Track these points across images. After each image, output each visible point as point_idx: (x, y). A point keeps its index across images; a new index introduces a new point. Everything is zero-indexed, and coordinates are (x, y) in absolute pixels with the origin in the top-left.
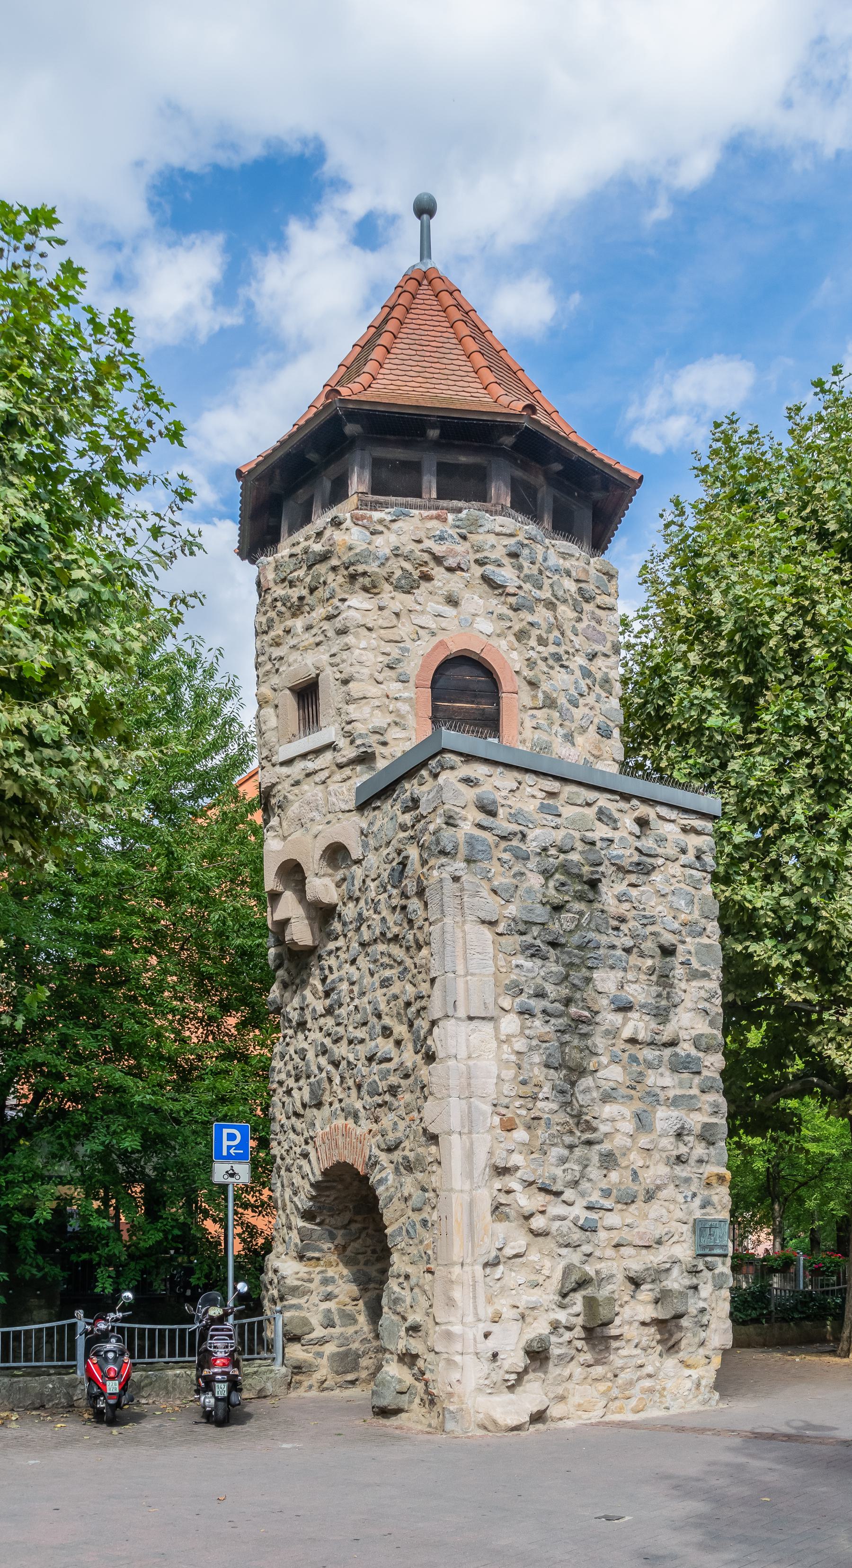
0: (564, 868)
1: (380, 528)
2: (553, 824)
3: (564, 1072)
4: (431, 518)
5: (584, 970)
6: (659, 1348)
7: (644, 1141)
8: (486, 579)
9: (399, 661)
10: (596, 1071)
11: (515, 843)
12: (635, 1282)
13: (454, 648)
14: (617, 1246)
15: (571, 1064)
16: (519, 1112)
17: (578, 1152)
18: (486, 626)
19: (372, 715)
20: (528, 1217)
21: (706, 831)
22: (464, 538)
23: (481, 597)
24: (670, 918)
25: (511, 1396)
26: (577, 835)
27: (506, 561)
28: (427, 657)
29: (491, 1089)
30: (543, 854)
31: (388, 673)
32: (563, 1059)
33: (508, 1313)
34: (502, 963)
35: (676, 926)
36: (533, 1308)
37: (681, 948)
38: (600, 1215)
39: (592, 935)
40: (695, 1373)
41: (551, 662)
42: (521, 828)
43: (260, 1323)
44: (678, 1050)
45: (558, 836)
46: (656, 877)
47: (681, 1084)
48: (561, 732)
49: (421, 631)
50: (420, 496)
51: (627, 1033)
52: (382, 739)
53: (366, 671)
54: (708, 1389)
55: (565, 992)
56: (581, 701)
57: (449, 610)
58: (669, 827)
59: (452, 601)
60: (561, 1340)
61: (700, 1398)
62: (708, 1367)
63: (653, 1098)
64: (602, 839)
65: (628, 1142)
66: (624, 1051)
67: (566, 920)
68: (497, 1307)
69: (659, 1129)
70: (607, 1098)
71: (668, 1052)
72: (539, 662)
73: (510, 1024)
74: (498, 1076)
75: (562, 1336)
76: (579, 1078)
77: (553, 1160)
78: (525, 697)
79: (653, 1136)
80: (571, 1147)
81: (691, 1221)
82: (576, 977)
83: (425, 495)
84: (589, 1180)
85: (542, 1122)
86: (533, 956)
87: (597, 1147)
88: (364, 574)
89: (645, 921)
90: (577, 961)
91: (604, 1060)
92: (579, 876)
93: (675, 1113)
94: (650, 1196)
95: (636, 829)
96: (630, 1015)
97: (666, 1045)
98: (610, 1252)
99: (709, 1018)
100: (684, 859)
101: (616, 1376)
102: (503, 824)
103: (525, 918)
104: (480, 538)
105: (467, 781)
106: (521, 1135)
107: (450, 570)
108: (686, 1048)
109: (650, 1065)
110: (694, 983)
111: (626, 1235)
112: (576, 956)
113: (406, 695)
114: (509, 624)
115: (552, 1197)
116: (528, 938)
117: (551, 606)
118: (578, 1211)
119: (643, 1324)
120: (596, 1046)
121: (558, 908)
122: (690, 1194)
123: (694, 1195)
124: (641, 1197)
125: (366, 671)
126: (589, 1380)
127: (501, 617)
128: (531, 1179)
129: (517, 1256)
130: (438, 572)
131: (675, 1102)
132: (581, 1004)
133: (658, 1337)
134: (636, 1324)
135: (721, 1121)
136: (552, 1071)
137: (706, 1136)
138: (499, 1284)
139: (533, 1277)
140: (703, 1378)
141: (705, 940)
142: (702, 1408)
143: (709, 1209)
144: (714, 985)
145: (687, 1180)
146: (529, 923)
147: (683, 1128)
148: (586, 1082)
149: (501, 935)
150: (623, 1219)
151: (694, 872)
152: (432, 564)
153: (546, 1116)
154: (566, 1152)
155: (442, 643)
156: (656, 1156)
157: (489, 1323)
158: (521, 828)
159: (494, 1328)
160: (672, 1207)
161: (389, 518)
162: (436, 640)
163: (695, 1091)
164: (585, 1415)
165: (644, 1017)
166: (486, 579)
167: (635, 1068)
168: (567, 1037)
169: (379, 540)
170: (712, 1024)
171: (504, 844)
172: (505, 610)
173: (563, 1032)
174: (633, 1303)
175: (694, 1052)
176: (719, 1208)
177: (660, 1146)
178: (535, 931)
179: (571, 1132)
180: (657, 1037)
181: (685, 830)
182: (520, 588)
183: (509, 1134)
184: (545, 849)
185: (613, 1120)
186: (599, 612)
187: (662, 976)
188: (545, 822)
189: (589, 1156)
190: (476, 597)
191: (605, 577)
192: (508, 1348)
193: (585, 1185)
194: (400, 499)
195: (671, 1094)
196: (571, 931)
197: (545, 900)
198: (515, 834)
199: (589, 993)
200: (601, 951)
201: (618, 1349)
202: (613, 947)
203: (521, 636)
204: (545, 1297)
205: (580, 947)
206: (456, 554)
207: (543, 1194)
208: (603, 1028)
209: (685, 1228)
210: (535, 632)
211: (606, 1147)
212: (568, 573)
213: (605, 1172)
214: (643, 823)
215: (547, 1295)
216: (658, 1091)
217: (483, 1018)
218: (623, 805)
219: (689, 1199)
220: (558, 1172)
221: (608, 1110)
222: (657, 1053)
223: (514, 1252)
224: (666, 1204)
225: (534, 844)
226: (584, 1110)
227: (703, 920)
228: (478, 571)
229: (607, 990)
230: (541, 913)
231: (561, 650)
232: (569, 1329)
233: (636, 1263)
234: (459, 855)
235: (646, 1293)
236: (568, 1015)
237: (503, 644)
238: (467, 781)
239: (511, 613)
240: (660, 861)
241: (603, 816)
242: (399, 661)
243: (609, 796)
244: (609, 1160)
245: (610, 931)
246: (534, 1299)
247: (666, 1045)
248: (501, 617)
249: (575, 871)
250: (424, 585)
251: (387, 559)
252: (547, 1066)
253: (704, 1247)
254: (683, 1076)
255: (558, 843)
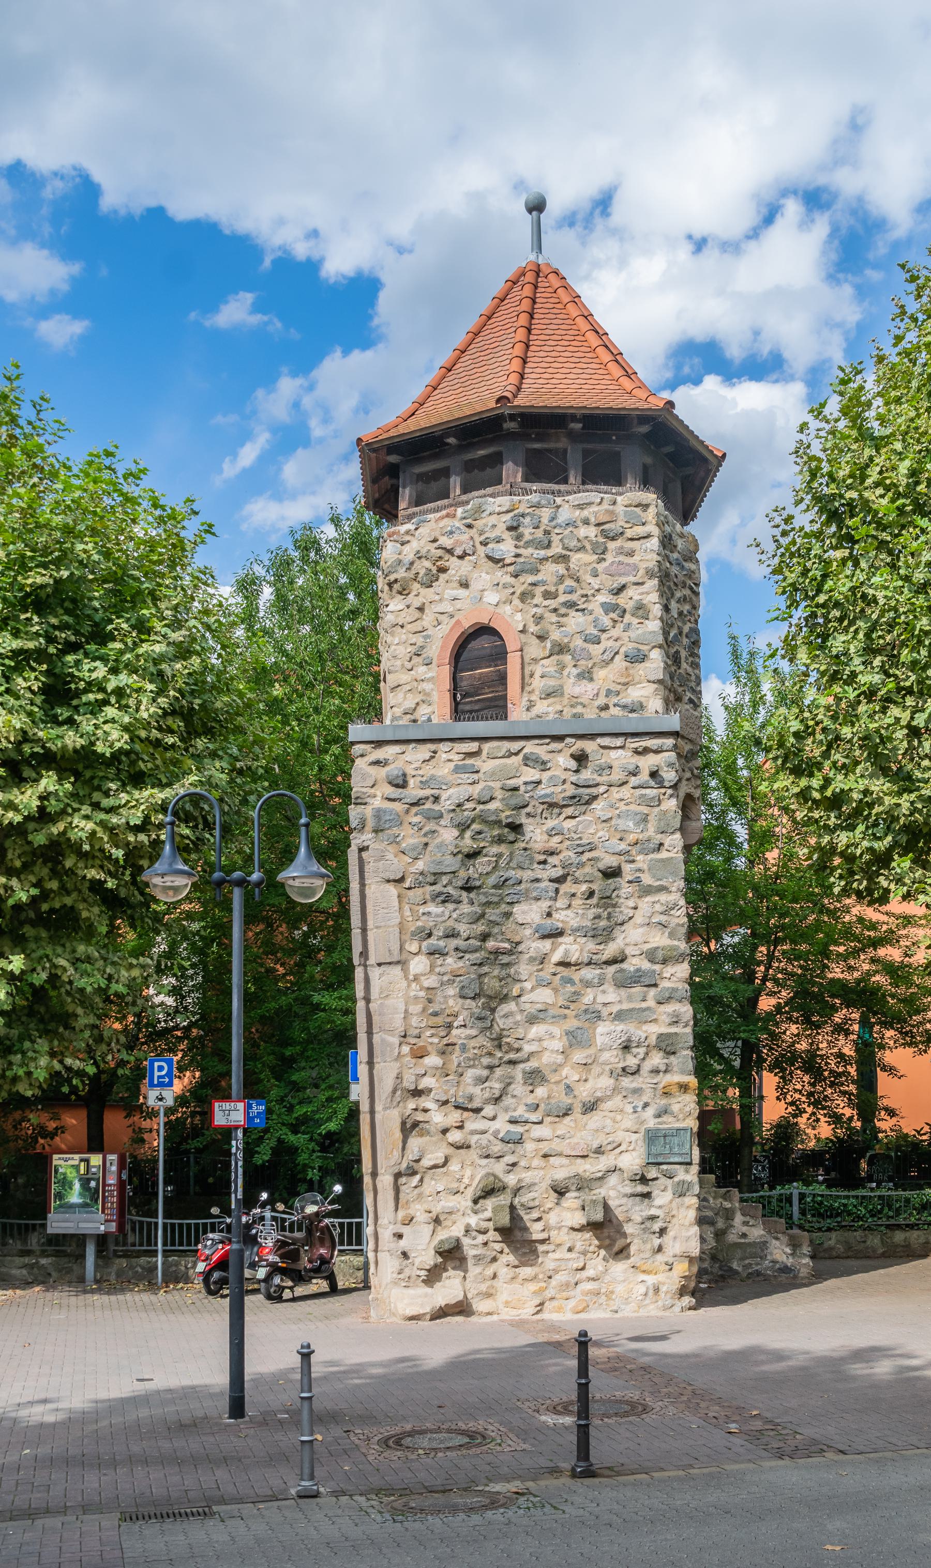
0: (482, 818)
1: (407, 538)
2: (469, 781)
3: (483, 1000)
4: (442, 518)
5: (503, 906)
6: (603, 1252)
7: (579, 1056)
8: (489, 558)
9: (422, 647)
10: (519, 996)
11: (428, 805)
12: (560, 1192)
13: (467, 623)
14: (545, 1156)
15: (489, 992)
16: (430, 1040)
17: (498, 1072)
18: (492, 597)
19: (405, 698)
20: (445, 1131)
21: (665, 748)
22: (470, 526)
23: (487, 573)
24: (615, 841)
25: (429, 1290)
26: (498, 785)
27: (507, 535)
28: (445, 638)
29: (398, 1023)
30: (458, 810)
31: (416, 660)
32: (481, 989)
33: (421, 1217)
34: (408, 913)
35: (623, 846)
36: (450, 1213)
37: (627, 868)
38: (526, 1128)
39: (511, 873)
40: (651, 1279)
41: (563, 610)
42: (433, 792)
43: (359, 1225)
44: (624, 966)
45: (476, 791)
46: (598, 805)
47: (630, 998)
48: (575, 671)
49: (441, 617)
50: (447, 496)
51: (556, 957)
52: (412, 717)
53: (399, 663)
54: (669, 1296)
55: (480, 928)
56: (604, 636)
57: (462, 593)
58: (614, 754)
59: (465, 585)
60: (474, 1242)
61: (660, 1303)
62: (670, 1274)
63: (595, 1016)
64: (526, 783)
65: (560, 1059)
66: (555, 975)
67: (482, 864)
68: (411, 1212)
69: (599, 1044)
70: (532, 1020)
71: (612, 969)
72: (547, 615)
73: (419, 965)
74: (406, 1011)
75: (474, 1238)
76: (499, 1004)
77: (469, 1081)
78: (535, 649)
79: (591, 1051)
80: (491, 1068)
81: (642, 1130)
82: (493, 914)
83: (452, 496)
84: (514, 1096)
85: (457, 1047)
86: (444, 902)
87: (522, 1066)
88: (396, 581)
89: (580, 849)
90: (496, 899)
91: (528, 985)
92: (498, 823)
93: (621, 1027)
94: (590, 1107)
95: (573, 764)
96: (560, 940)
97: (609, 963)
98: (536, 1162)
99: (667, 931)
100: (634, 781)
101: (550, 1277)
102: (414, 791)
103: (432, 870)
104: (484, 521)
105: (377, 763)
106: (433, 1060)
107: (461, 557)
108: (634, 963)
109: (588, 984)
110: (649, 899)
111: (556, 1145)
112: (493, 895)
113: (430, 675)
114: (512, 590)
115: (471, 1114)
116: (438, 888)
117: (563, 559)
118: (501, 1125)
119: (573, 1229)
120: (519, 973)
121: (473, 855)
122: (641, 1104)
123: (646, 1105)
124: (578, 1108)
125: (399, 663)
126: (520, 1280)
127: (505, 586)
128: (444, 1099)
129: (435, 1167)
130: (453, 562)
131: (619, 1016)
132: (500, 938)
133: (596, 1242)
134: (565, 1230)
135: (686, 1031)
136: (469, 1001)
137: (666, 1045)
138: (417, 1191)
139: (455, 1185)
140: (664, 1284)
141: (664, 855)
142: (661, 1314)
143: (665, 1118)
144: (676, 897)
145: (637, 1091)
146: (438, 875)
147: (629, 1040)
148: (504, 1008)
149: (410, 888)
150: (554, 1131)
151: (648, 791)
152: (447, 556)
153: (460, 1042)
154: (485, 1073)
155: (458, 622)
156: (596, 1069)
157: (399, 1225)
158: (433, 792)
159: (405, 1230)
160: (619, 1117)
161: (412, 527)
162: (454, 620)
163: (651, 1003)
164: (515, 1312)
165: (579, 940)
166: (489, 558)
167: (570, 988)
168: (486, 969)
169: (406, 548)
170: (672, 935)
171: (414, 810)
172: (509, 579)
173: (481, 965)
174: (557, 1209)
175: (646, 965)
176: (681, 1116)
177: (601, 1060)
178: (445, 880)
179: (490, 1054)
180: (594, 957)
181: (637, 752)
182: (517, 556)
183: (421, 1060)
184: (459, 805)
185: (540, 1040)
186: (631, 544)
187: (602, 898)
188: (460, 781)
189: (513, 1074)
190: (483, 575)
191: (638, 510)
192: (419, 1248)
193: (508, 1101)
194: (432, 505)
195: (615, 1009)
196: (487, 873)
197: (456, 851)
198: (427, 798)
199: (510, 925)
200: (523, 886)
201: (548, 1252)
202: (537, 880)
203: (524, 597)
204: (463, 1203)
205: (495, 887)
206: (462, 543)
207: (460, 1111)
208: (527, 956)
209: (634, 1137)
210: (539, 590)
211: (533, 1064)
212: (586, 522)
213: (531, 1088)
214: (581, 759)
215: (465, 1202)
216: (599, 1007)
217: (390, 963)
218: (555, 746)
219: (639, 1109)
220: (477, 1091)
221: (536, 1031)
222: (598, 971)
223: (431, 1163)
224: (612, 1114)
225: (448, 802)
226: (505, 1033)
227: (659, 836)
228: (481, 550)
229: (529, 921)
230: (451, 863)
231: (574, 597)
232: (485, 1232)
233: (561, 1171)
234: (366, 828)
235: (571, 1200)
236: (485, 949)
237: (508, 609)
238: (377, 763)
239: (512, 580)
240: (602, 789)
241: (528, 761)
242: (422, 647)
243: (537, 741)
244: (535, 1077)
245: (536, 866)
246: (451, 1204)
247: (609, 963)
248: (505, 586)
249: (493, 818)
250: (443, 577)
251: (412, 563)
252: (463, 997)
253: (657, 1155)
254: (633, 990)
255: (476, 796)
